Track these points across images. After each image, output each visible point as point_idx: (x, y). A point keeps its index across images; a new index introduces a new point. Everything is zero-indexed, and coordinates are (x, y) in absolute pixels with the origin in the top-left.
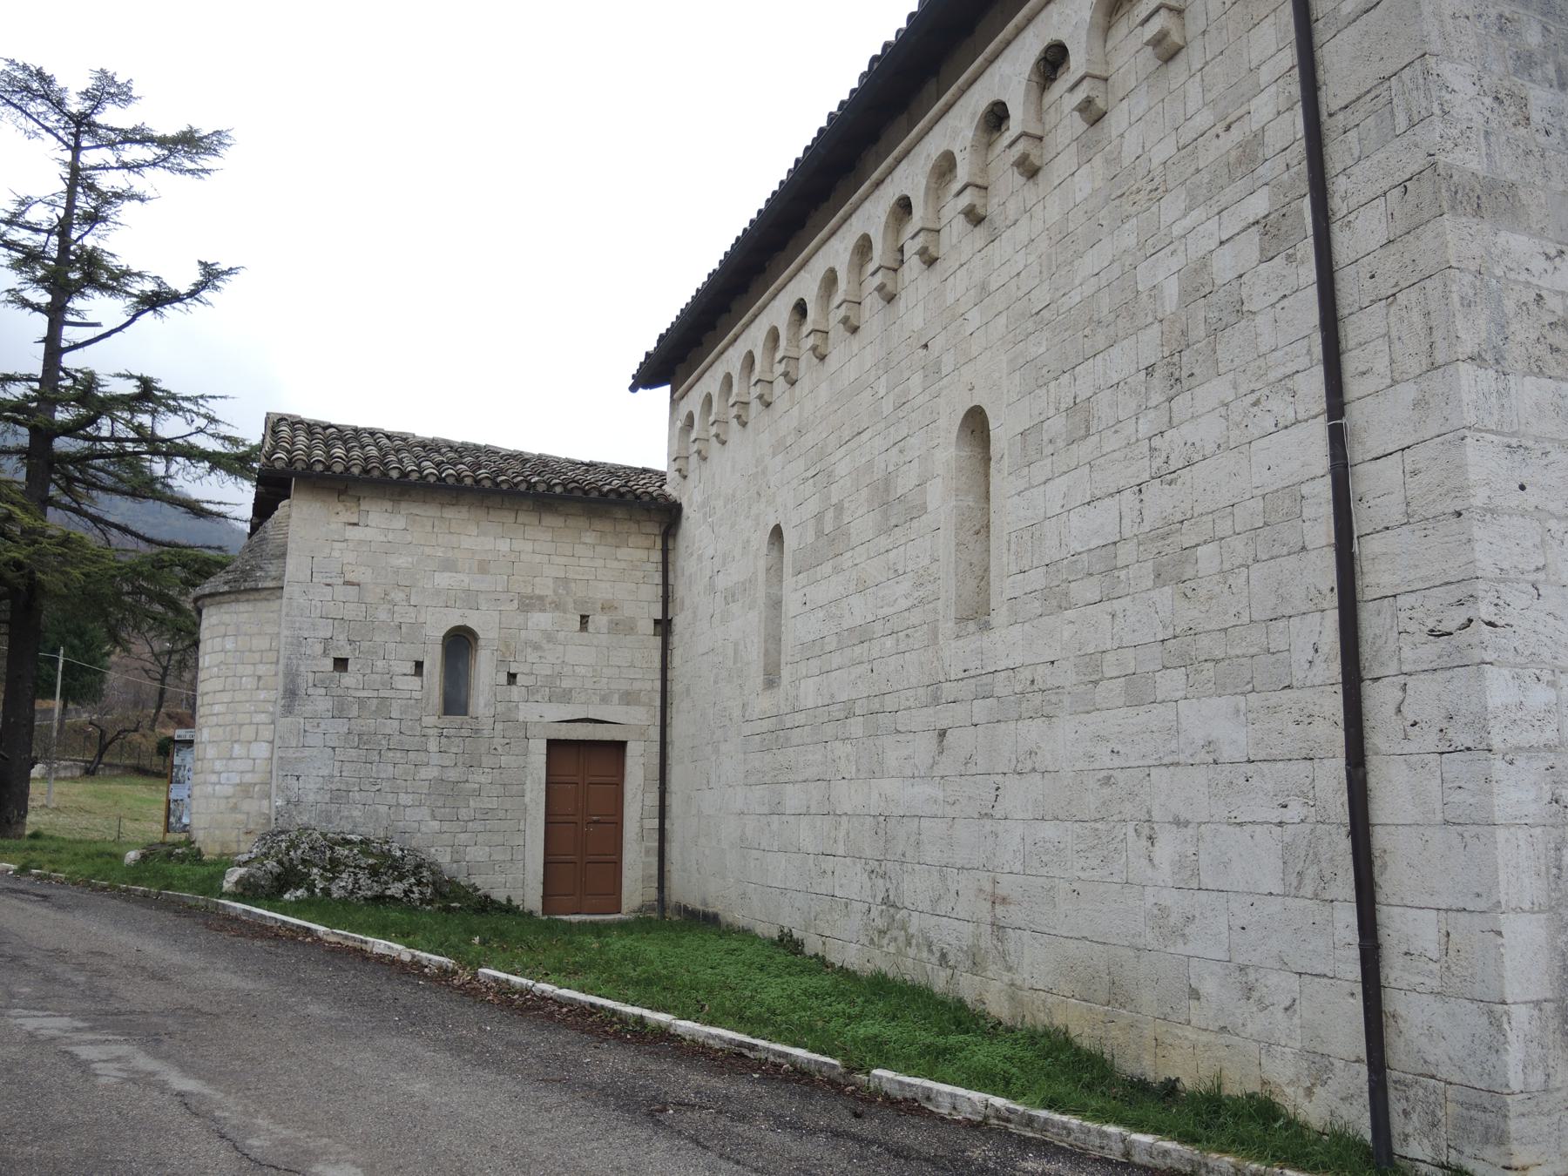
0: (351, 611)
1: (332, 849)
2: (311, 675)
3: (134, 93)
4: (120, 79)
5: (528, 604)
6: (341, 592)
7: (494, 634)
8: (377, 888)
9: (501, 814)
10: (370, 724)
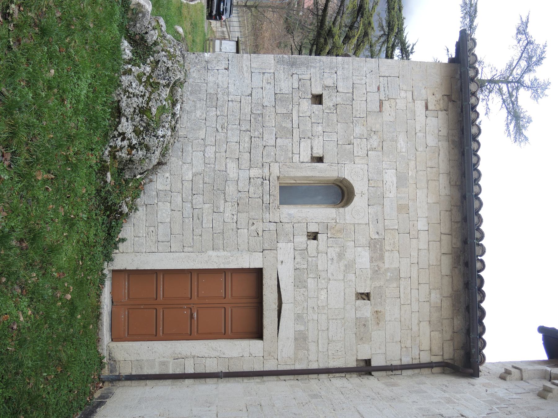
0: (359, 106)
1: (168, 85)
2: (308, 77)
3: (540, 100)
4: (546, 92)
5: (376, 247)
6: (374, 98)
7: (349, 219)
8: (128, 111)
9: (197, 231)
10: (271, 122)
